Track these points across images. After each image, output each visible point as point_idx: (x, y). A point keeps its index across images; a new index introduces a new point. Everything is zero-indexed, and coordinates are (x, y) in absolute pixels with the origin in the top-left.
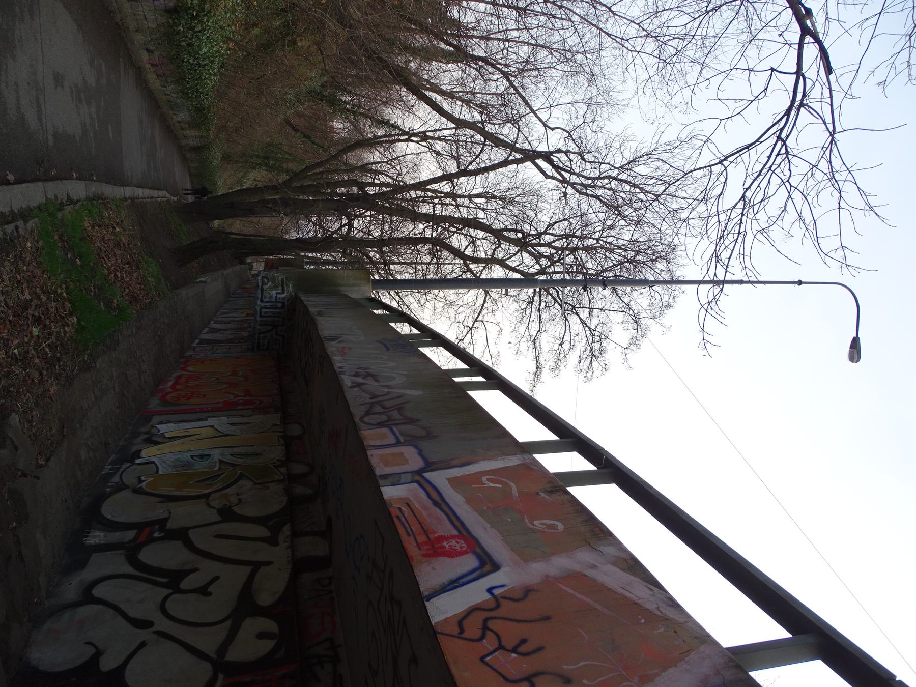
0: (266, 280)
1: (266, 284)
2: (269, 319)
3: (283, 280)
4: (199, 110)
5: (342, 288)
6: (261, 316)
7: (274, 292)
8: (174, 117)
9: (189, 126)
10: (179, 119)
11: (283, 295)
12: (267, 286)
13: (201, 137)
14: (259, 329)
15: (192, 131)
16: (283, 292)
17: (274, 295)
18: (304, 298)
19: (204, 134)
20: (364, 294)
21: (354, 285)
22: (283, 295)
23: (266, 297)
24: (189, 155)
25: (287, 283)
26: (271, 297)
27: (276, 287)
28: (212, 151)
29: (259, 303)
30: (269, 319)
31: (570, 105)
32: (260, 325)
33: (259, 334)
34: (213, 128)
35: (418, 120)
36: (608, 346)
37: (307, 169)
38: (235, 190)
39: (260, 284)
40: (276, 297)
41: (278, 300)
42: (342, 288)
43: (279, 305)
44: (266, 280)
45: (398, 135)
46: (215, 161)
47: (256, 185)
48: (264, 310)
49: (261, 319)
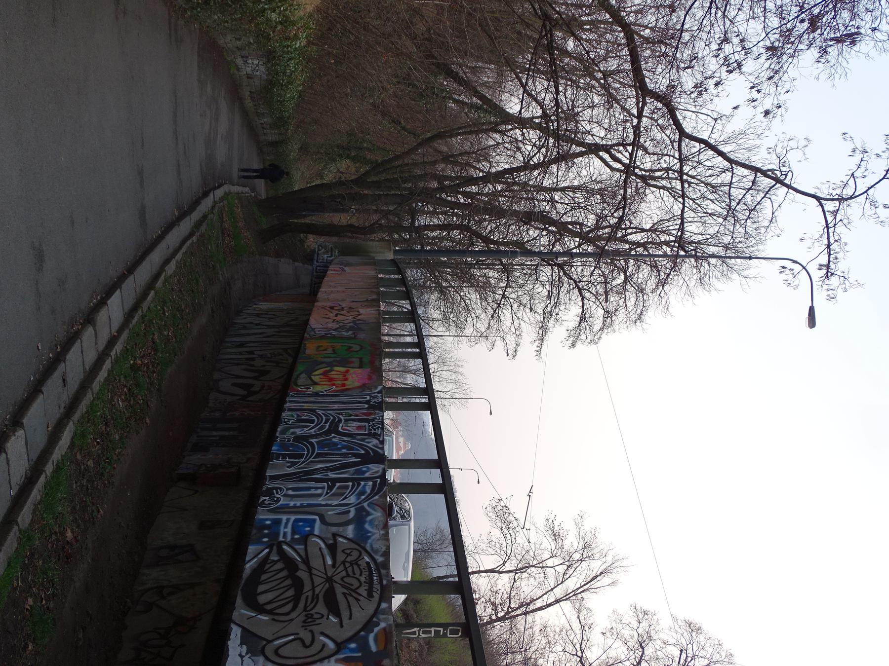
0: (320, 248)
3: (331, 247)
6: (316, 272)
7: (326, 256)
9: (270, 127)
16: (331, 256)
17: (326, 258)
26: (323, 259)
27: (327, 252)
29: (315, 263)
31: (535, 598)
33: (315, 284)
35: (684, 288)
36: (582, 613)
38: (314, 184)
39: (317, 250)
42: (372, 254)
44: (320, 248)
47: (340, 178)
48: (318, 268)
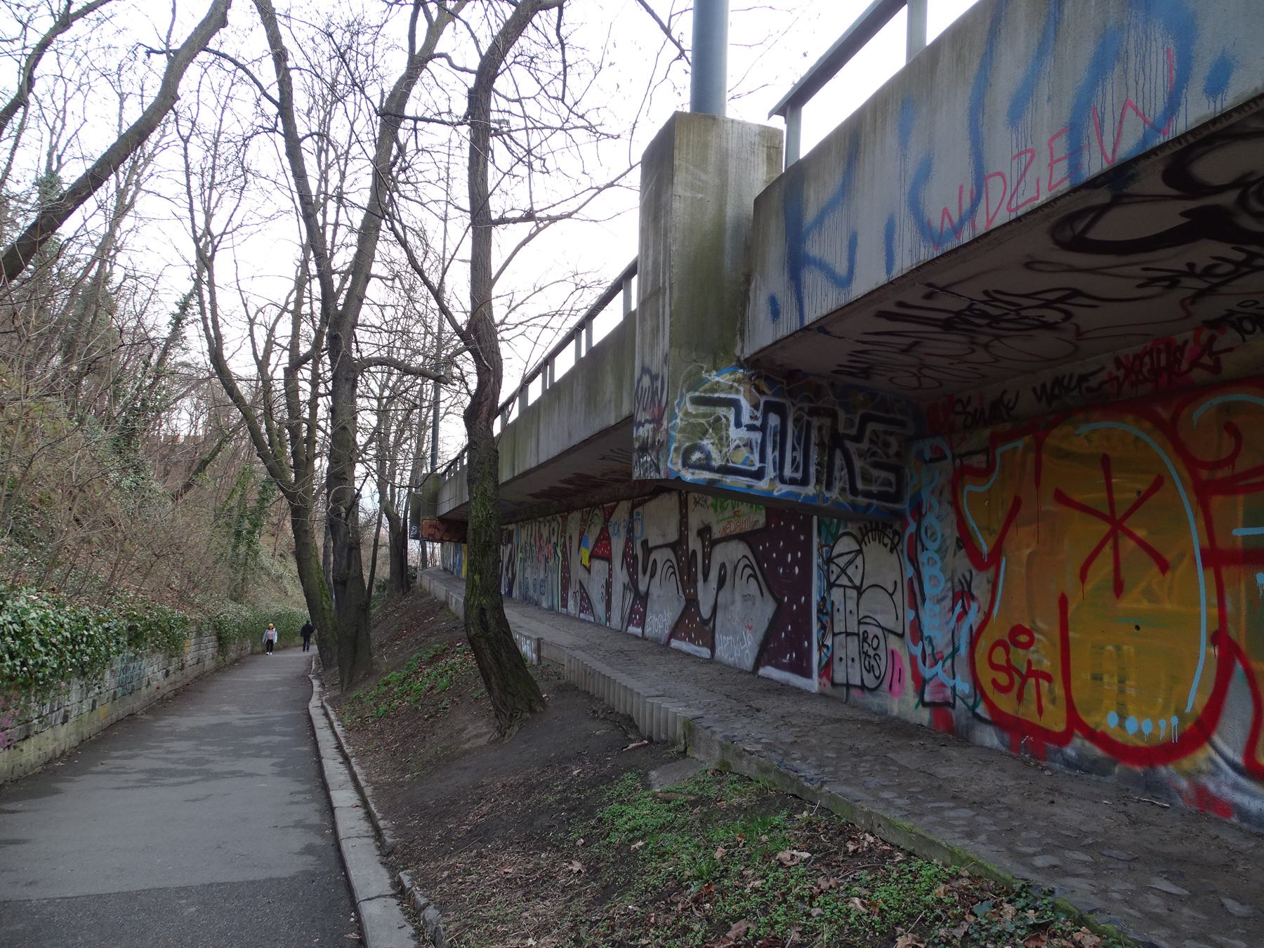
0: (696, 456)
1: (708, 456)
2: (814, 457)
3: (697, 401)
4: (135, 637)
5: (730, 211)
6: (804, 482)
8: (154, 684)
10: (160, 675)
11: (745, 404)
12: (715, 454)
13: (199, 634)
14: (843, 490)
15: (187, 650)
16: (735, 404)
18: (748, 350)
19: (194, 628)
20: (752, 144)
21: (722, 172)
22: (745, 404)
23: (747, 461)
24: (233, 655)
25: (707, 386)
26: (749, 445)
28: (226, 617)
29: (763, 485)
30: (814, 457)
32: (829, 486)
33: (854, 491)
34: (179, 614)
37: (263, 456)
39: (707, 475)
40: (751, 428)
41: (758, 423)
42: (730, 211)
43: (774, 420)
44: (696, 456)
45: (201, 303)
46: (244, 614)
48: (788, 472)
49: (813, 480)
